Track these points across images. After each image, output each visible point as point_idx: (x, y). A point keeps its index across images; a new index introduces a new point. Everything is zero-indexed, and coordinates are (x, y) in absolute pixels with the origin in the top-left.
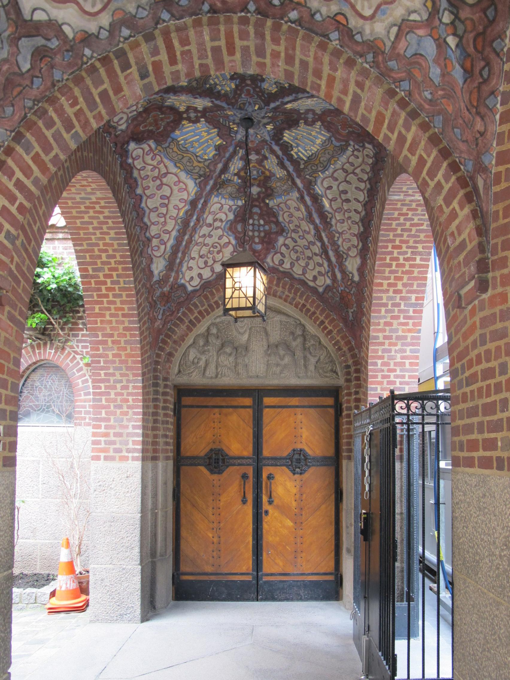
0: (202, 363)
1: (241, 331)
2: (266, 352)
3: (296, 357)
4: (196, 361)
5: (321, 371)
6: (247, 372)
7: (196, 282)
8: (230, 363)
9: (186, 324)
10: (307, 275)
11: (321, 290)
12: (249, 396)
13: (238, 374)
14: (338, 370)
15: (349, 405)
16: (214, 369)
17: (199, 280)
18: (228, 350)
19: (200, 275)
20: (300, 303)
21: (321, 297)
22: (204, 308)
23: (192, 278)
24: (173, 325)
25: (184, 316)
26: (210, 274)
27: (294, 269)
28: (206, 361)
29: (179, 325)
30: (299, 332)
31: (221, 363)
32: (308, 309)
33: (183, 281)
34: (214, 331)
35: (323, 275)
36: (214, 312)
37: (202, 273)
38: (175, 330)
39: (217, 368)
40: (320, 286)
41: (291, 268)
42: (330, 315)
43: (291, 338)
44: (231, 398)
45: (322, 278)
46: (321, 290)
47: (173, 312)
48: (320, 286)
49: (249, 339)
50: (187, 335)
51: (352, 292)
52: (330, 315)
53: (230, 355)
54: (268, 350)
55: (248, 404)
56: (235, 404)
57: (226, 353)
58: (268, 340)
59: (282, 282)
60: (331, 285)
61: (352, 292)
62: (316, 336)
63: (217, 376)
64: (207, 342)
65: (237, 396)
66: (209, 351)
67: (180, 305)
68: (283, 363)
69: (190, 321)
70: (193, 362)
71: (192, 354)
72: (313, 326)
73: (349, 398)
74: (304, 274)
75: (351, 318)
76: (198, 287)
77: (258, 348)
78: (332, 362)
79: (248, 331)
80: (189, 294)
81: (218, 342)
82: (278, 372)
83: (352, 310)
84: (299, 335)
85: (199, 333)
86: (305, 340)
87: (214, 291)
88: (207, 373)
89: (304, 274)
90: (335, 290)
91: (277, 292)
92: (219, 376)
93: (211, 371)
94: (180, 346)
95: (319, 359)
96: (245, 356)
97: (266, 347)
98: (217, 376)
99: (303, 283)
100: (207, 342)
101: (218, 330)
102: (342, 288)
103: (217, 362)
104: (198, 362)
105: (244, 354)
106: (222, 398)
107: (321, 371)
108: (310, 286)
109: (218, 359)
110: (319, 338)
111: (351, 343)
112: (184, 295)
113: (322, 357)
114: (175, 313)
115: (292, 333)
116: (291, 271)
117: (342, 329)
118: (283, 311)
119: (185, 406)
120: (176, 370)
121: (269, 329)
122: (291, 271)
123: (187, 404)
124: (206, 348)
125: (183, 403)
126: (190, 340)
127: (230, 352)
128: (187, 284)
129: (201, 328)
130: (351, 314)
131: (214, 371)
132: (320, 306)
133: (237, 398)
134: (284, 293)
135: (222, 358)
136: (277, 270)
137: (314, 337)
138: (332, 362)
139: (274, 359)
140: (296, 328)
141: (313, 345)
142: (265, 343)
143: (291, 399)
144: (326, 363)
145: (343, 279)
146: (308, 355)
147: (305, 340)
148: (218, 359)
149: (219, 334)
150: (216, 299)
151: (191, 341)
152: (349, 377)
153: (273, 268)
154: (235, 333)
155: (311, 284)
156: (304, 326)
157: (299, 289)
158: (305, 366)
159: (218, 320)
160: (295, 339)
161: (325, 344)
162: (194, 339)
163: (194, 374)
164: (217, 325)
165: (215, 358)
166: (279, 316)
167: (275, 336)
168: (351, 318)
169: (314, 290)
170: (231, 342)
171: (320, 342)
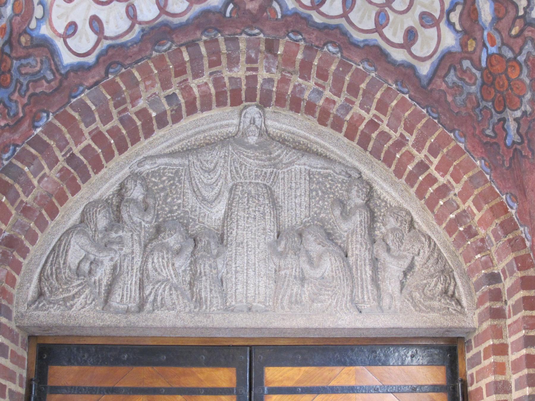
0: (102, 274)
1: (209, 194)
2: (273, 246)
3: (351, 260)
4: (86, 267)
5: (417, 295)
6: (224, 297)
7: (84, 41)
8: (177, 275)
9: (59, 166)
10: (387, 32)
11: (425, 69)
12: (227, 365)
13: (199, 302)
14: (462, 292)
15: (500, 378)
16: (135, 288)
17: (93, 37)
18: (173, 240)
19: (96, 23)
20: (362, 119)
21: (424, 90)
22: (108, 126)
23: (72, 27)
24: (18, 158)
25: (51, 137)
26: (125, 24)
27: (352, 16)
28: (114, 268)
29: (34, 157)
30: (357, 199)
31: (152, 273)
32: (383, 133)
33: (45, 30)
34: (137, 192)
35: (436, 23)
36: (138, 147)
37: (102, 17)
38: (22, 172)
39: (142, 288)
40: (423, 60)
41: (345, 15)
42: (450, 140)
43: (337, 212)
44: (180, 369)
45: (433, 31)
46: (425, 69)
47: (19, 122)
48: (423, 60)
49: (228, 215)
50: (63, 199)
51: (522, 58)
52: (450, 140)
53: (178, 252)
54: (278, 243)
55: (225, 385)
56: (191, 382)
57: (169, 249)
58: (277, 218)
59: (319, 55)
60: (458, 49)
61: (522, 58)
62: (400, 208)
63: (141, 308)
64: (117, 221)
65: (198, 364)
66: (121, 241)
67: (38, 102)
68: (317, 273)
69: (71, 159)
70: (78, 272)
71: (76, 252)
72: (393, 184)
73: (500, 359)
74: (379, 28)
75: (513, 135)
76: (91, 59)
77: (252, 235)
78: (446, 273)
79: (227, 194)
80: (66, 76)
81: (147, 222)
82: (305, 298)
83: (518, 114)
84: (357, 207)
85: (96, 197)
86: (373, 218)
87: (136, 74)
88: (116, 300)
89: (379, 28)
90: (466, 64)
91: (302, 91)
92: (148, 306)
93: (126, 294)
94: (42, 225)
95: (411, 267)
96: (218, 255)
97: (273, 236)
98: (141, 308)
99: (376, 55)
100: (117, 221)
101: (148, 190)
102: (493, 50)
103: (143, 270)
104: (90, 272)
105: (215, 252)
106: (156, 369)
107: (417, 295)
108: (393, 63)
109: (145, 262)
110: (408, 213)
111: (506, 211)
112: (50, 77)
113: (419, 261)
114: (25, 126)
115: (342, 203)
116: (343, 22)
117: (481, 174)
118: (314, 147)
119: (56, 390)
120: (32, 291)
121: (279, 191)
122: (343, 22)
123: (62, 383)
124: (114, 235)
125: (51, 382)
126: (71, 212)
127: (177, 247)
128: (59, 43)
129: (103, 185)
130: (512, 126)
131: (136, 294)
132: (417, 116)
133: (194, 369)
134: (320, 93)
135: (157, 260)
136: (307, 19)
137: (397, 211)
138: (446, 273)
139: (291, 265)
140: (348, 191)
141: (394, 230)
142: (270, 225)
143: (338, 369)
144: (432, 276)
145: (497, 19)
146: (383, 255)
147: (373, 218)
148: (145, 262)
149: (151, 201)
150: (142, 103)
151: (75, 217)
152: (498, 305)
153: (296, 14)
154: (191, 200)
155: (399, 55)
156: (369, 184)
157: (365, 75)
158: (375, 281)
159: (147, 167)
160: (346, 215)
161: (424, 228)
162: (83, 214)
163: (81, 300)
164: (144, 179)
165: (138, 260)
166: (304, 160)
167: (296, 208)
168: (513, 135)
169: (406, 73)
170: (184, 224)
171: (412, 224)
